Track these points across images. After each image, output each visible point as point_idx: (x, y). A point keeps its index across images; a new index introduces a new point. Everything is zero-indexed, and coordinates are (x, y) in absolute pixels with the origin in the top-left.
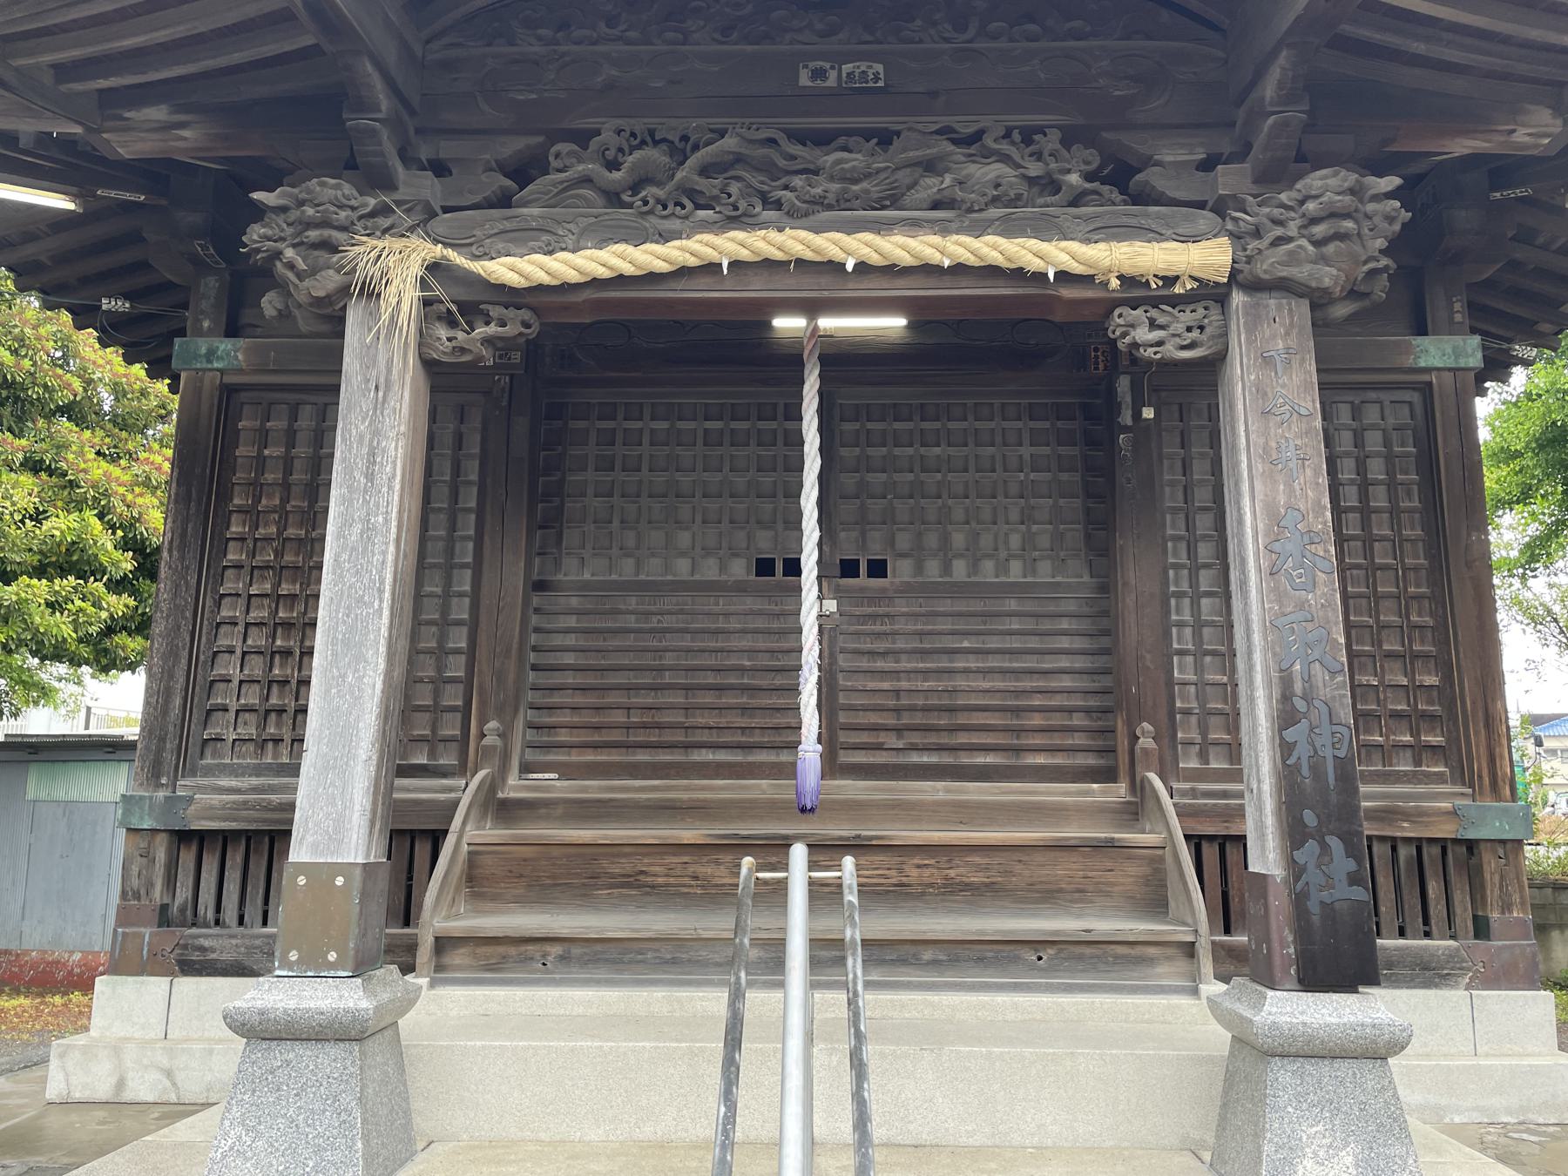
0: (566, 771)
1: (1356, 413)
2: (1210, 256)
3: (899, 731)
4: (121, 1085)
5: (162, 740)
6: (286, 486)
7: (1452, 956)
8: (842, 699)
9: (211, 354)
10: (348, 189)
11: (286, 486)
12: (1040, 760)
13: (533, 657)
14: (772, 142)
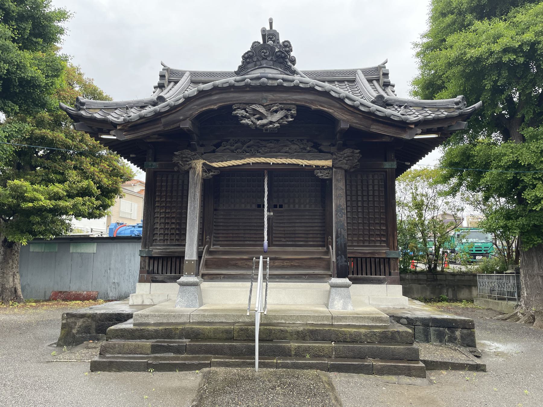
0: (222, 245)
1: (373, 177)
2: (328, 163)
3: (285, 238)
4: (143, 302)
5: (146, 240)
6: (166, 191)
7: (384, 279)
8: (274, 232)
9: (152, 165)
10: (190, 152)
11: (166, 191)
12: (311, 243)
13: (214, 224)
14: (258, 142)
